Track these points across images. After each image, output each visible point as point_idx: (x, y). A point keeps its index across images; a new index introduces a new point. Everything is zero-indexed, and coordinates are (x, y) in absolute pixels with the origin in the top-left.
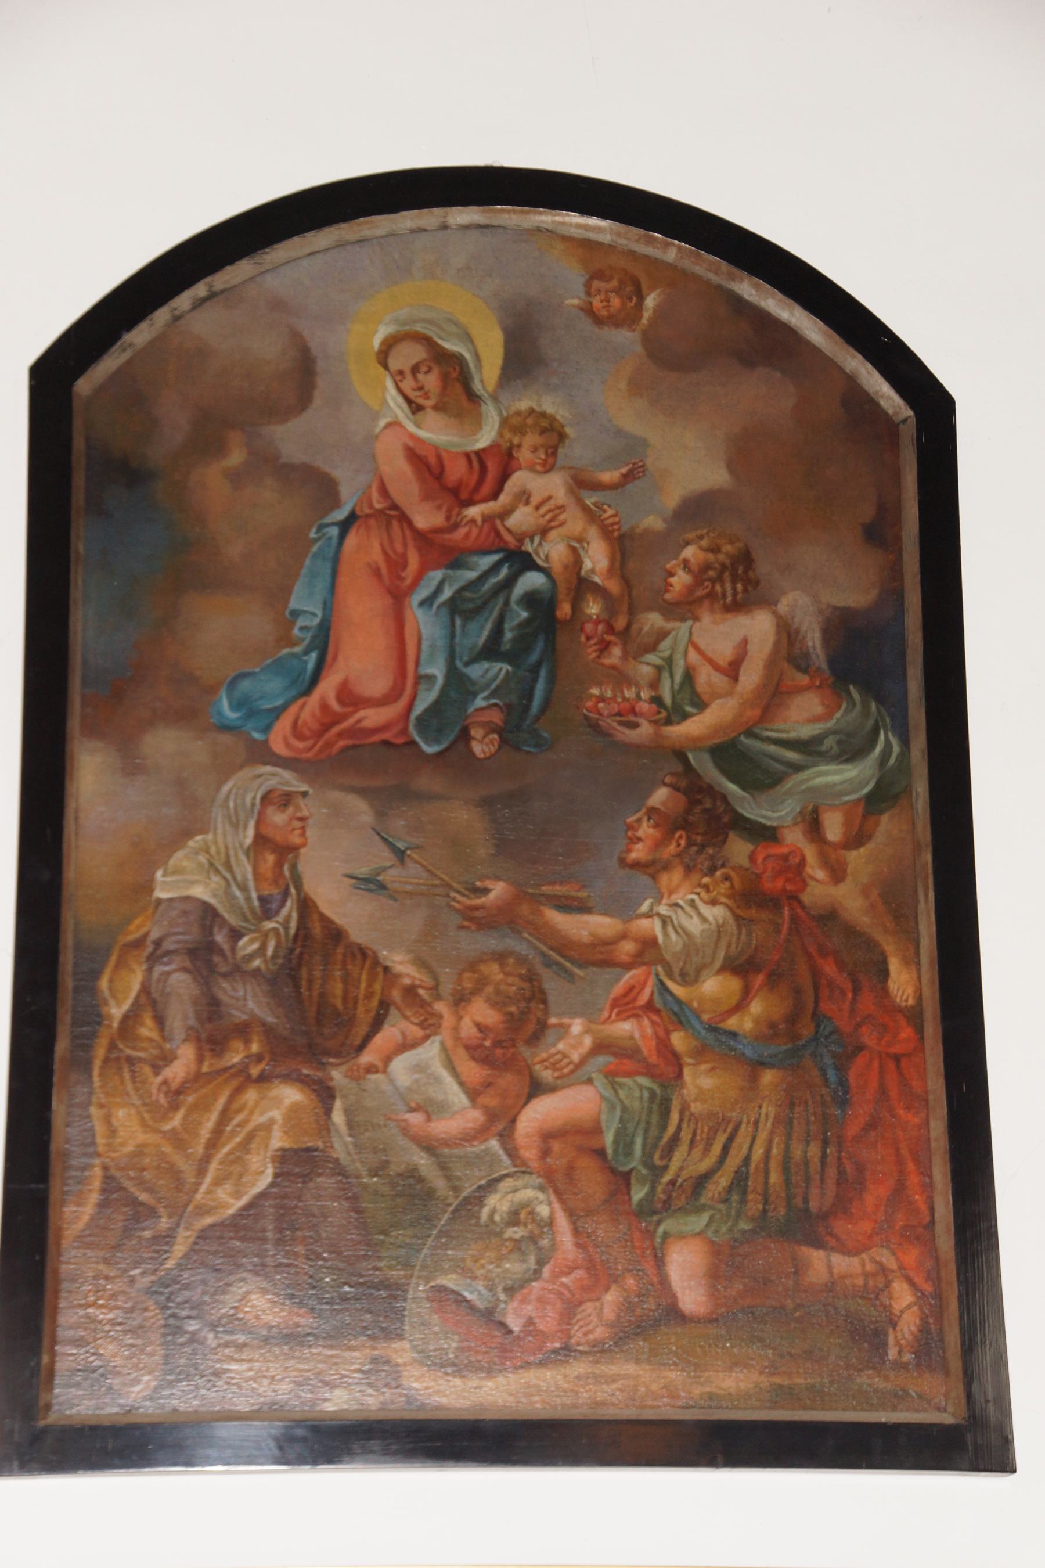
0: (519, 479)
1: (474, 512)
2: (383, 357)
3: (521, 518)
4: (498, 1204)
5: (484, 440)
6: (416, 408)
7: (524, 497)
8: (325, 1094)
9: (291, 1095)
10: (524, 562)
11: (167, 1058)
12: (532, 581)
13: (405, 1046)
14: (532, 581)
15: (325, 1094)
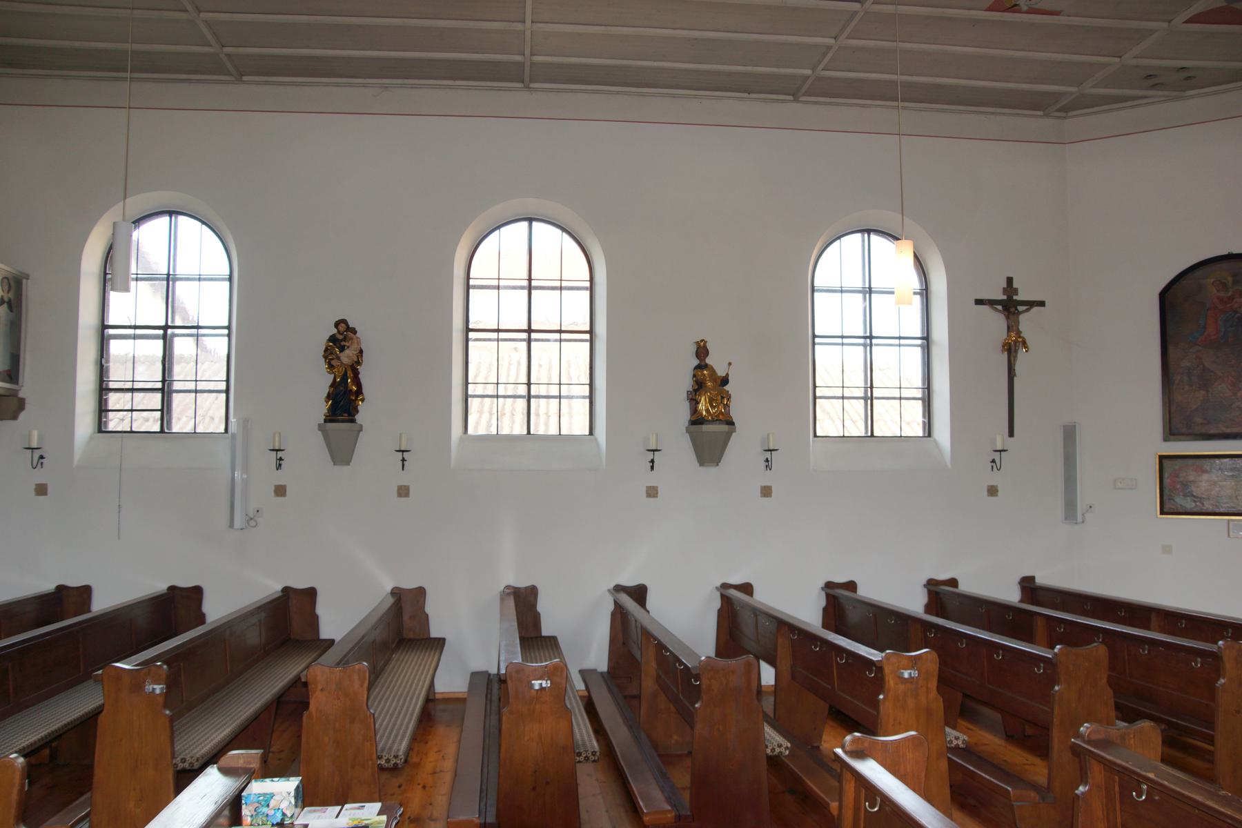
0: (1235, 300)
1: (1228, 306)
2: (1213, 284)
3: (1236, 306)
4: (1234, 406)
5: (1230, 294)
6: (1218, 291)
7: (1236, 302)
8: (1208, 391)
9: (1202, 392)
10: (1236, 312)
11: (1183, 389)
12: (1238, 315)
13: (1220, 384)
14: (1238, 315)
15: (1208, 391)
